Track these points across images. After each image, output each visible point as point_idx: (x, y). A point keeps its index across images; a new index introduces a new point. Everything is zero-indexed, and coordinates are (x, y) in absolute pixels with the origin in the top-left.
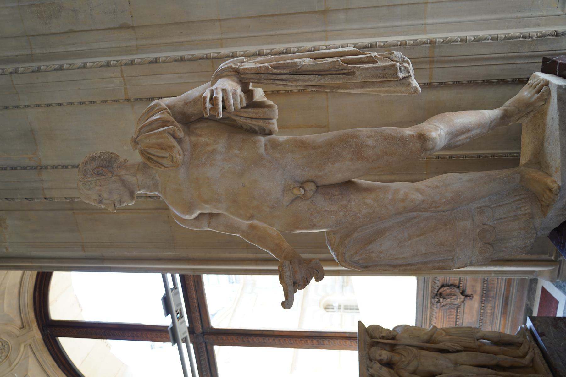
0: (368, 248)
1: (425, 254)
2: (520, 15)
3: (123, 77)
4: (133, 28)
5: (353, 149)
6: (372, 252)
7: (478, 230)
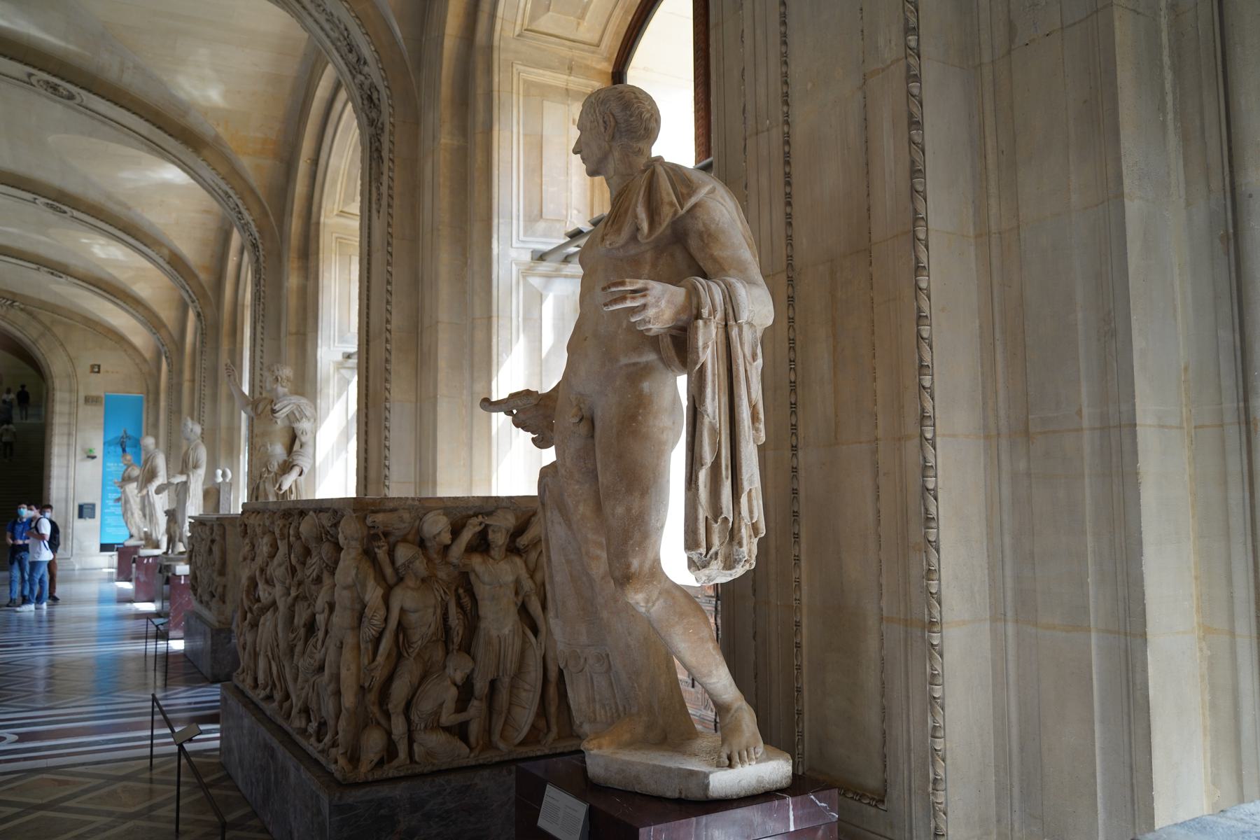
2: (1016, 791)
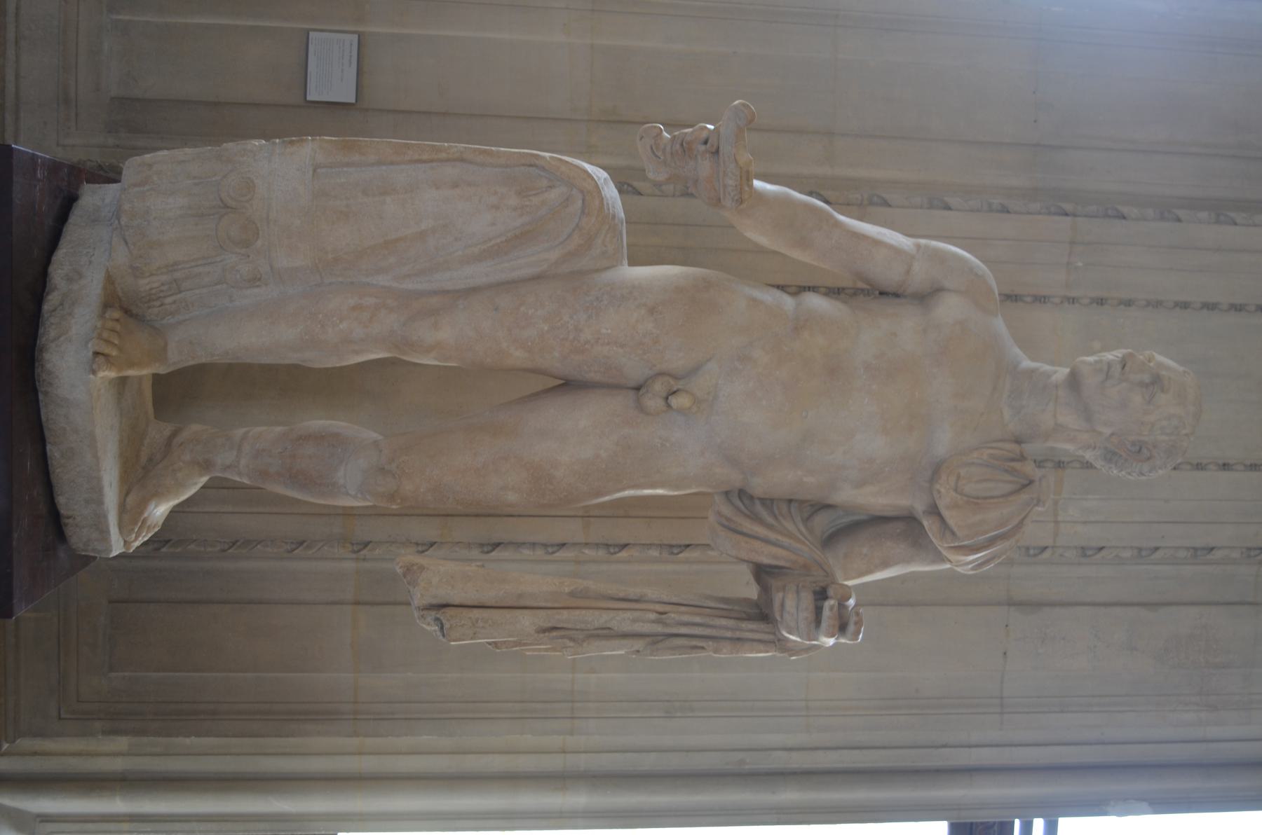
3: (1057, 522)
4: (1011, 603)
7: (259, 243)
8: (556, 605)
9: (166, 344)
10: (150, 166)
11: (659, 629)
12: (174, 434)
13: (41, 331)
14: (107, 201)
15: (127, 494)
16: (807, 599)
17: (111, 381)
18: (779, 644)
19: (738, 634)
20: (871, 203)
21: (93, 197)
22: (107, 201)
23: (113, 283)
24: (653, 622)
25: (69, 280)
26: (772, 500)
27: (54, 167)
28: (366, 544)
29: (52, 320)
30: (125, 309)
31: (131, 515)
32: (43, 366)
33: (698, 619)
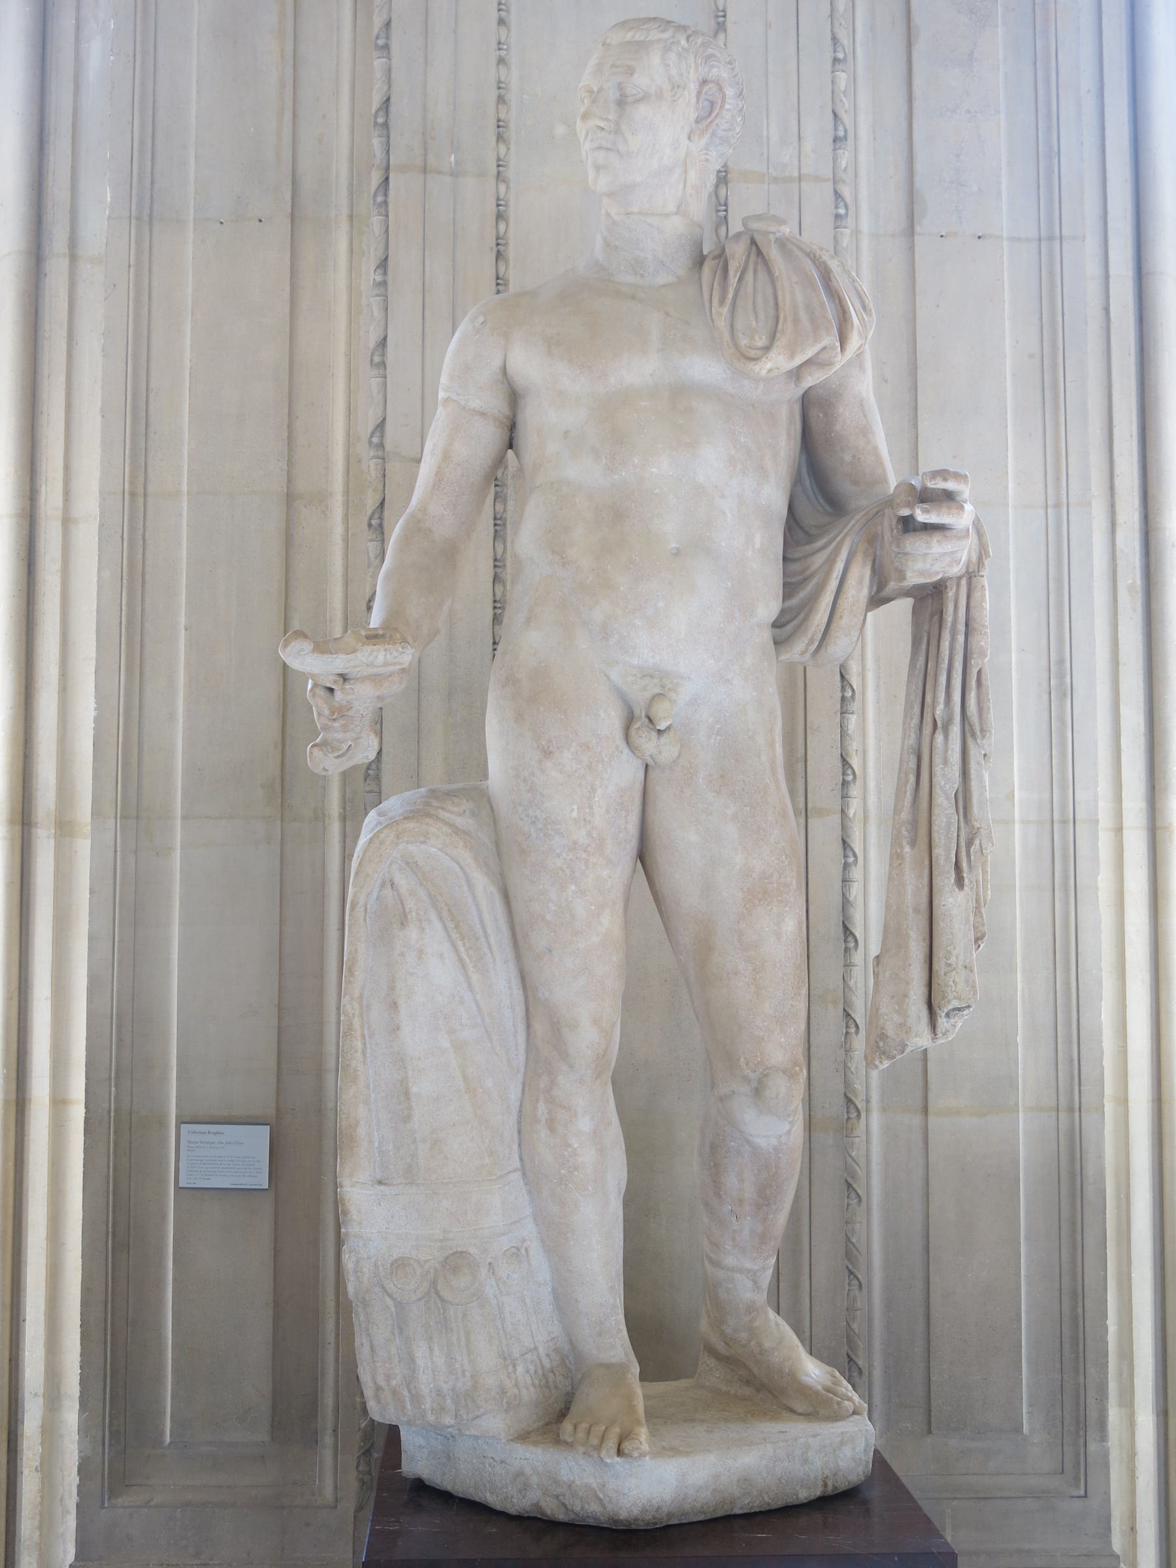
0: (433, 916)
1: (407, 1094)
4: (910, 231)
5: (776, 875)
6: (422, 930)
8: (927, 862)
9: (602, 1365)
10: (378, 1389)
11: (956, 729)
12: (712, 1351)
13: (592, 1522)
14: (422, 1442)
15: (792, 1411)
16: (915, 544)
17: (652, 1434)
18: (971, 576)
19: (961, 627)
20: (381, 445)
21: (418, 1461)
22: (422, 1442)
23: (529, 1433)
24: (946, 737)
25: (526, 1486)
26: (786, 585)
27: (382, 1510)
28: (849, 1101)
29: (577, 1508)
30: (558, 1412)
31: (820, 1407)
32: (636, 1519)
33: (943, 680)
